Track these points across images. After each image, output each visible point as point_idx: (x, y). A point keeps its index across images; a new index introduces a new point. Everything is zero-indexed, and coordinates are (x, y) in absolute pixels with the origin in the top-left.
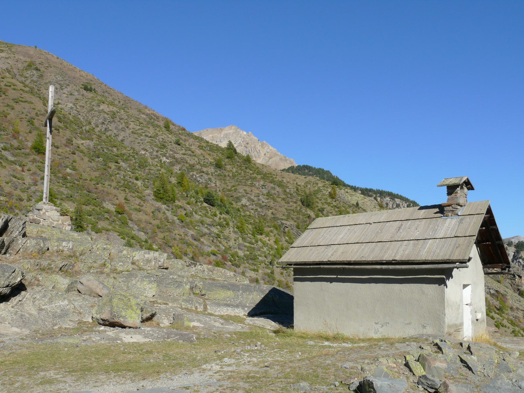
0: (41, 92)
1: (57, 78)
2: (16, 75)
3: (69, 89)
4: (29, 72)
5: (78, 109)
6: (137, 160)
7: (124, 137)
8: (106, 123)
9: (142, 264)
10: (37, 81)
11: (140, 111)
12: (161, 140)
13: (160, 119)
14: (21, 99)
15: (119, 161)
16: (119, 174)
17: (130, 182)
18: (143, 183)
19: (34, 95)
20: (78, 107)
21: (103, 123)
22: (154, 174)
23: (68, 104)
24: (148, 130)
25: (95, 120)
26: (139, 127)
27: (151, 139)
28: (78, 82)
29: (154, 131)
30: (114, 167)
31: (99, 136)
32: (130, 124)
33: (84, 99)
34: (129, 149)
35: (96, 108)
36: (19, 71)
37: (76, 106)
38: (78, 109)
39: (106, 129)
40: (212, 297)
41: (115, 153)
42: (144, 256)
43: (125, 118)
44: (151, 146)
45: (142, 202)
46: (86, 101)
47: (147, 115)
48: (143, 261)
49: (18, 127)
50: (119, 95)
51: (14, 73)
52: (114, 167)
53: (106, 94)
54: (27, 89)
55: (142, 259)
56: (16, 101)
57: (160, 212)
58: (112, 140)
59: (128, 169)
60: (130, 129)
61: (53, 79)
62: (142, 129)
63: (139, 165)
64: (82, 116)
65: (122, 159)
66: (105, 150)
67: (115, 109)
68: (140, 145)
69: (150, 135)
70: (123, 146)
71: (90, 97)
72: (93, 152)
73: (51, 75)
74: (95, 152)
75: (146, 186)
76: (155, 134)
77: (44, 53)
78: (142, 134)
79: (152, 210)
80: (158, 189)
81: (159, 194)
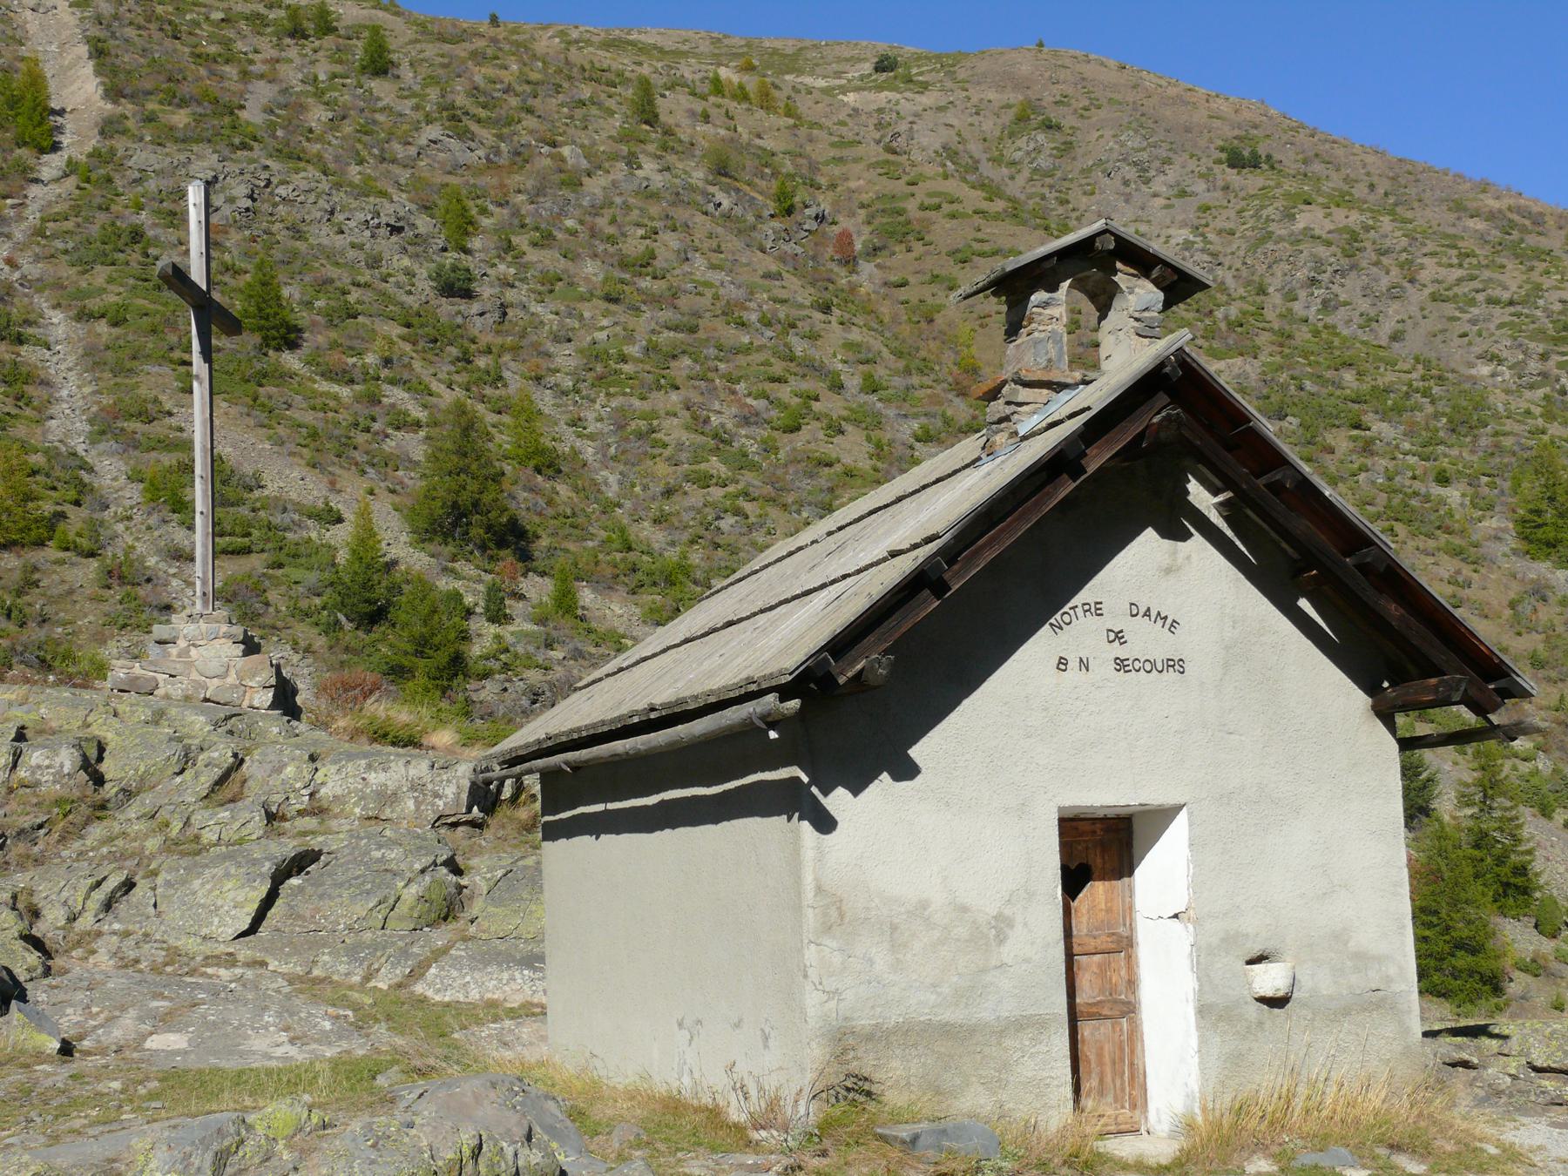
0: (1071, 206)
1: (1123, 145)
2: (978, 162)
3: (1172, 174)
4: (1022, 142)
5: (1211, 243)
6: (1444, 402)
7: (1403, 321)
8: (1325, 277)
9: (357, 810)
10: (1055, 168)
11: (1458, 207)
12: (1557, 307)
13: (1550, 222)
14: (976, 246)
15: (1369, 418)
16: (1367, 471)
17: (1416, 494)
18: (1470, 491)
19: (1024, 223)
20: (1211, 236)
21: (1313, 282)
22: (1516, 448)
23: (1171, 231)
24: (1496, 276)
25: (1279, 274)
26: (1459, 273)
27: (1512, 309)
28: (1203, 143)
29: (1525, 277)
30: (1344, 444)
31: (1281, 333)
32: (1422, 267)
33: (1233, 201)
34: (1407, 367)
35: (1279, 230)
36: (987, 144)
37: (1202, 235)
38: (1211, 243)
39: (1325, 303)
40: (493, 929)
41: (1348, 391)
42: (364, 779)
43: (1398, 248)
44: (1515, 339)
45: (1467, 571)
46: (1238, 207)
47: (1491, 216)
48: (361, 799)
49: (974, 350)
50: (1370, 159)
51: (971, 157)
52: (1344, 444)
53: (1317, 167)
54: (999, 205)
55: (356, 791)
56: (959, 256)
57: (1544, 599)
58: (1337, 342)
59: (1407, 446)
60: (1424, 286)
61: (1111, 149)
62: (1473, 278)
63: (1450, 421)
64: (1230, 268)
65: (1380, 408)
66: (1308, 384)
67: (1355, 218)
68: (1470, 344)
69: (1506, 296)
70: (1381, 359)
71: (1256, 192)
72: (1258, 398)
73: (1102, 136)
74: (1268, 398)
75: (1482, 504)
76: (1529, 286)
77: (1067, 62)
78: (1474, 299)
79: (1512, 595)
80: (1531, 506)
81: (1540, 526)
